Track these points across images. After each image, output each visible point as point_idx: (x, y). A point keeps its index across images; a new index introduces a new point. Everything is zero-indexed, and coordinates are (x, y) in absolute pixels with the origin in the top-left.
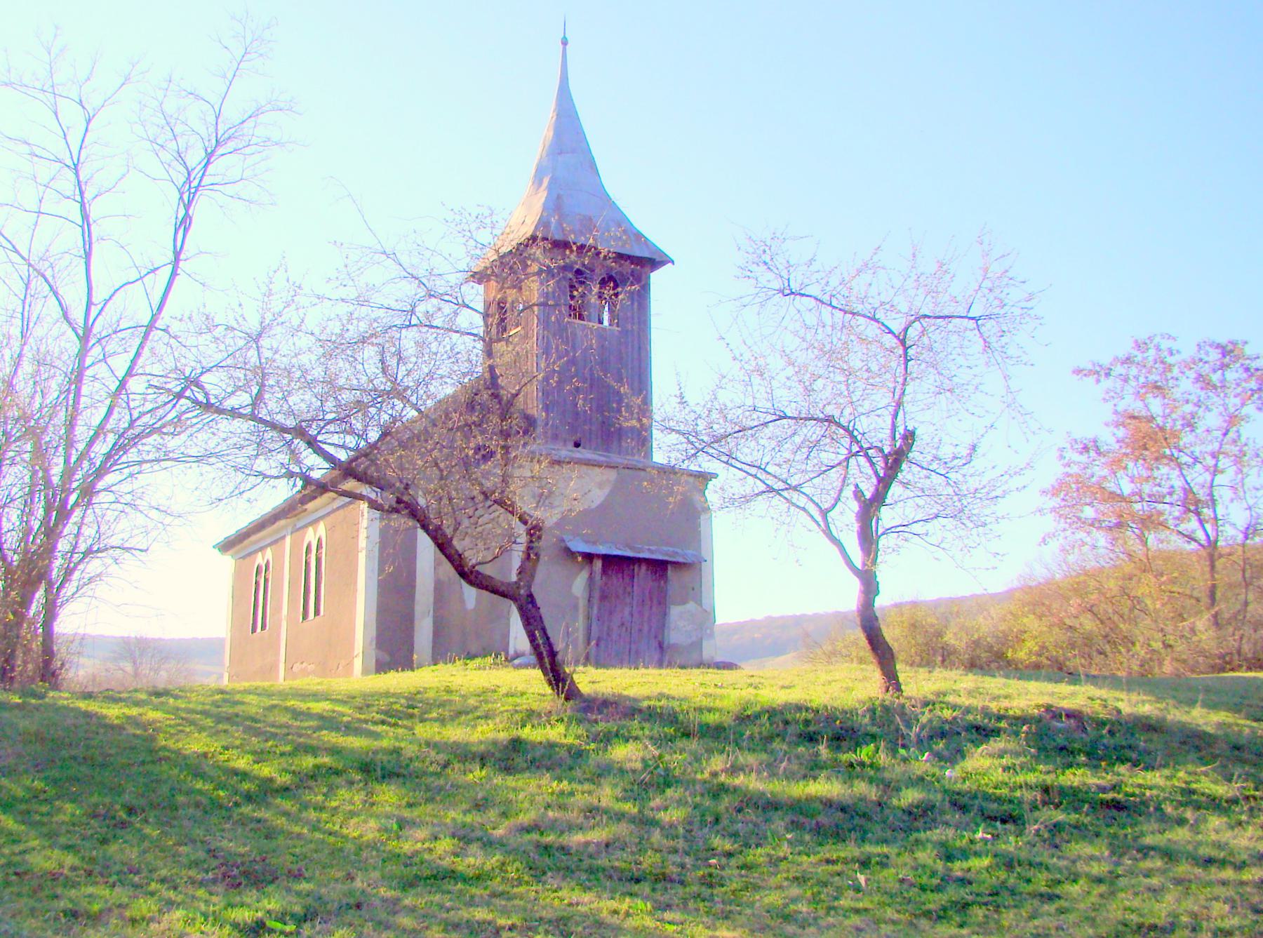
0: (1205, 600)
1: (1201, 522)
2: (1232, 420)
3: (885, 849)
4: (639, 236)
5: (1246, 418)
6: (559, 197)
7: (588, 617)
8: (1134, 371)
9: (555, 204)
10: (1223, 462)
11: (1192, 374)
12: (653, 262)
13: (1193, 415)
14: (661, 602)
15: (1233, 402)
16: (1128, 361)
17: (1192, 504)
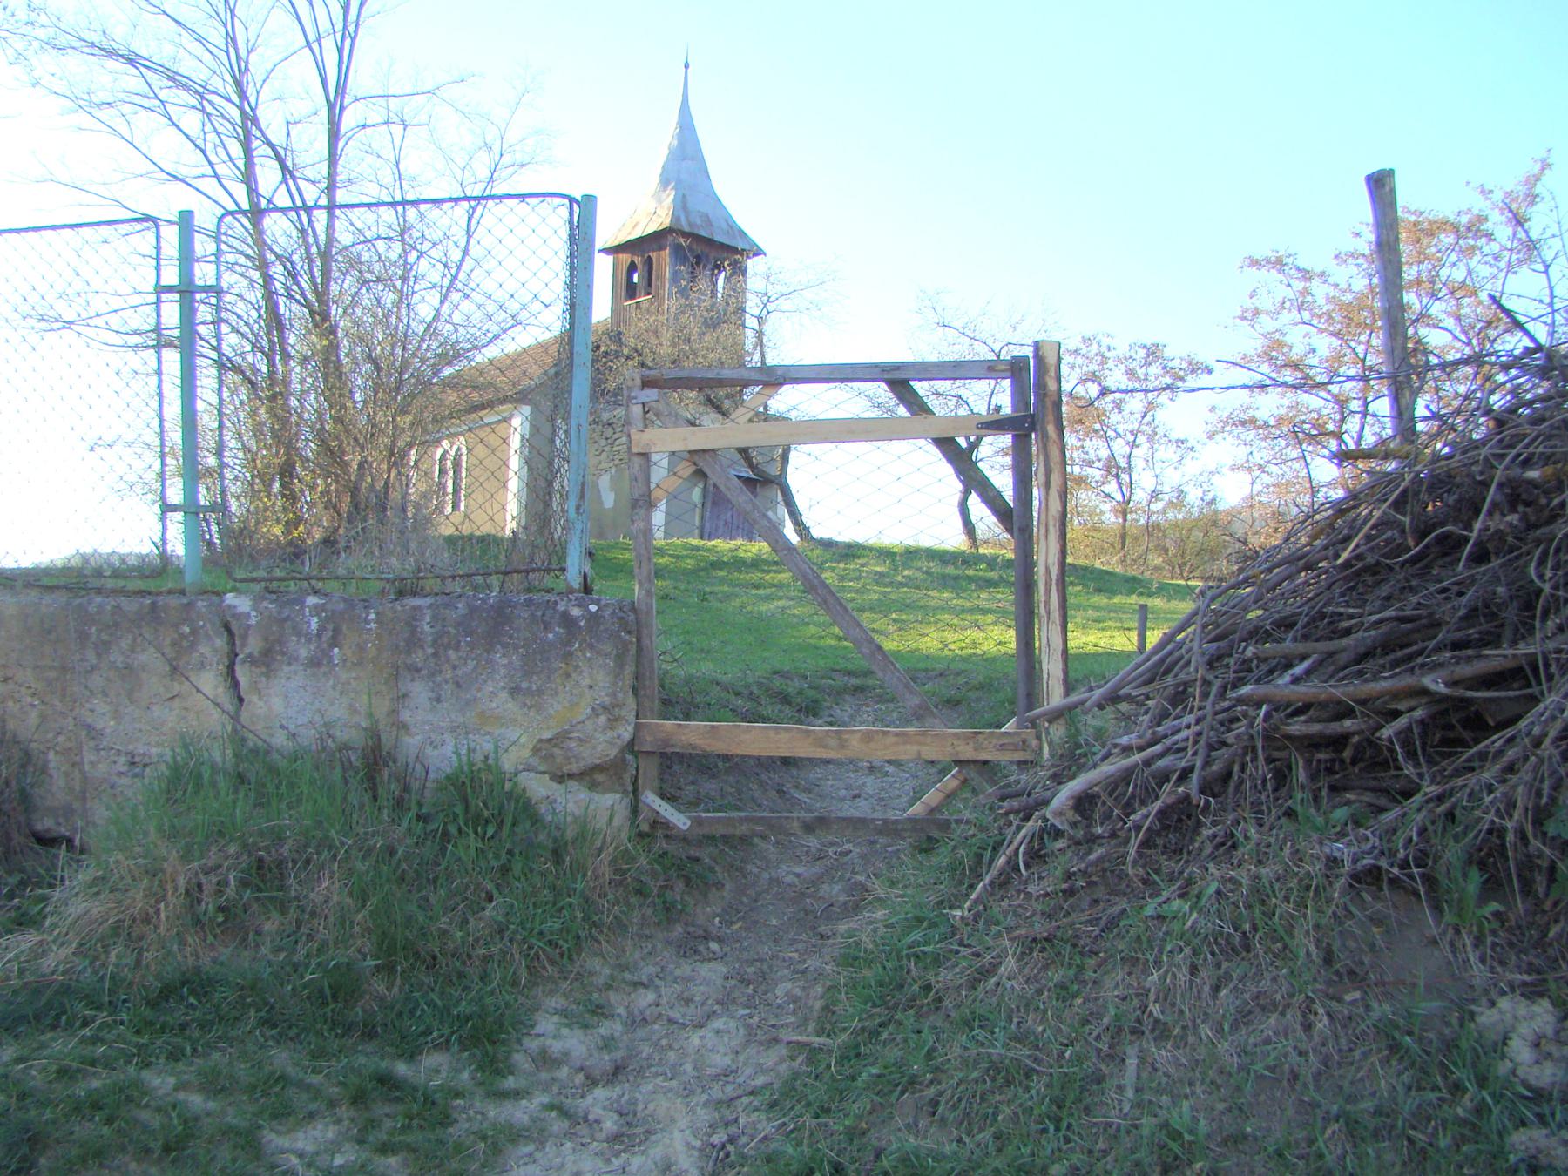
0: (1118, 546)
1: (1120, 484)
4: (742, 234)
6: (684, 196)
7: (702, 518)
8: (1079, 360)
9: (682, 204)
10: (1141, 439)
11: (1123, 368)
17: (1112, 468)
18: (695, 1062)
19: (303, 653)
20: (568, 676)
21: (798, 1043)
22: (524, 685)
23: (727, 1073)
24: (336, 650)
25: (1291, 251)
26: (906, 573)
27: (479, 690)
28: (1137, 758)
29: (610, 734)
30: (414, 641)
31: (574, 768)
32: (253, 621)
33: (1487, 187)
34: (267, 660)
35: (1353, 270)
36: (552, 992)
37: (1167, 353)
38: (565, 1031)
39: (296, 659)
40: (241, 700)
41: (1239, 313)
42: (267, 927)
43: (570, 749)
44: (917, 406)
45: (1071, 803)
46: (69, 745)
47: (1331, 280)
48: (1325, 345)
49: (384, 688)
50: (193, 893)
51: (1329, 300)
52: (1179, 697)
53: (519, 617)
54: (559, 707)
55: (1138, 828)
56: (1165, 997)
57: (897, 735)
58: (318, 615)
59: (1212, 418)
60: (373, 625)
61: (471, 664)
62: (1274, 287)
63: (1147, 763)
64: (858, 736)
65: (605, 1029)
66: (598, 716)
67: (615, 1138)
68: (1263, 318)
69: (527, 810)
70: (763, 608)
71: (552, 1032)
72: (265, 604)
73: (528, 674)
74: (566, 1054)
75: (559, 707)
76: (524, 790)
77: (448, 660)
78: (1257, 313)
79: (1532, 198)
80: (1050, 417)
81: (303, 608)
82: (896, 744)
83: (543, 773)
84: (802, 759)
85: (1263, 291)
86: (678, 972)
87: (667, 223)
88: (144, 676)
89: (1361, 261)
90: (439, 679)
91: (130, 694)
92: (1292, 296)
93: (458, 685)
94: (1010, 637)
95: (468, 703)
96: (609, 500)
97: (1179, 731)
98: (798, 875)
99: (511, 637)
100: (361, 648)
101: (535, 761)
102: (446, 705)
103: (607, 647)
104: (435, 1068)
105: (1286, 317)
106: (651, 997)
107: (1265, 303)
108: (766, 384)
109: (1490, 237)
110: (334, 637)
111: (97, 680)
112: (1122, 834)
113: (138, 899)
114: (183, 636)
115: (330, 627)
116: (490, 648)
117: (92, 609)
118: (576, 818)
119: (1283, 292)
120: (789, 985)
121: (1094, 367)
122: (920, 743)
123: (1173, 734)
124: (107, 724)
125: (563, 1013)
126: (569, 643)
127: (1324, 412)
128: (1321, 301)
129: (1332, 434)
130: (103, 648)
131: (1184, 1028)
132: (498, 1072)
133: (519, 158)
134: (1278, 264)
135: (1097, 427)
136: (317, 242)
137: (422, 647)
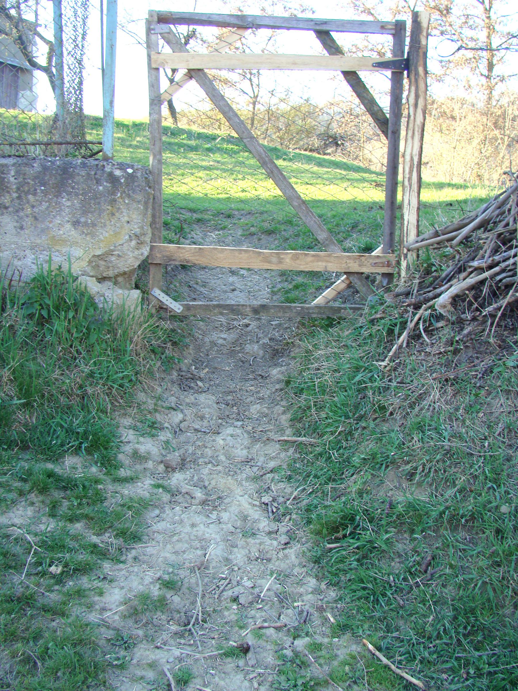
20: (113, 214)
22: (83, 220)
23: (248, 461)
26: (138, 139)
27: (51, 222)
28: (486, 274)
29: (136, 252)
31: (111, 273)
38: (141, 439)
43: (111, 262)
44: (333, 48)
45: (450, 300)
53: (78, 174)
54: (107, 235)
55: (493, 316)
57: (313, 256)
61: (45, 205)
63: (492, 277)
64: (290, 256)
65: (163, 436)
66: (131, 240)
67: (204, 503)
69: (83, 302)
71: (131, 440)
73: (85, 213)
74: (149, 453)
75: (107, 235)
76: (86, 287)
80: (421, 62)
82: (312, 262)
83: (92, 276)
84: (195, 265)
86: (187, 400)
90: (21, 214)
93: (36, 219)
94: (379, 196)
95: (43, 231)
97: (508, 259)
98: (225, 339)
99: (73, 188)
101: (88, 269)
102: (27, 232)
104: (73, 465)
106: (180, 416)
108: (240, 27)
116: (58, 195)
120: (258, 407)
122: (327, 261)
123: (504, 261)
125: (135, 428)
126: (113, 193)
137: (8, 192)
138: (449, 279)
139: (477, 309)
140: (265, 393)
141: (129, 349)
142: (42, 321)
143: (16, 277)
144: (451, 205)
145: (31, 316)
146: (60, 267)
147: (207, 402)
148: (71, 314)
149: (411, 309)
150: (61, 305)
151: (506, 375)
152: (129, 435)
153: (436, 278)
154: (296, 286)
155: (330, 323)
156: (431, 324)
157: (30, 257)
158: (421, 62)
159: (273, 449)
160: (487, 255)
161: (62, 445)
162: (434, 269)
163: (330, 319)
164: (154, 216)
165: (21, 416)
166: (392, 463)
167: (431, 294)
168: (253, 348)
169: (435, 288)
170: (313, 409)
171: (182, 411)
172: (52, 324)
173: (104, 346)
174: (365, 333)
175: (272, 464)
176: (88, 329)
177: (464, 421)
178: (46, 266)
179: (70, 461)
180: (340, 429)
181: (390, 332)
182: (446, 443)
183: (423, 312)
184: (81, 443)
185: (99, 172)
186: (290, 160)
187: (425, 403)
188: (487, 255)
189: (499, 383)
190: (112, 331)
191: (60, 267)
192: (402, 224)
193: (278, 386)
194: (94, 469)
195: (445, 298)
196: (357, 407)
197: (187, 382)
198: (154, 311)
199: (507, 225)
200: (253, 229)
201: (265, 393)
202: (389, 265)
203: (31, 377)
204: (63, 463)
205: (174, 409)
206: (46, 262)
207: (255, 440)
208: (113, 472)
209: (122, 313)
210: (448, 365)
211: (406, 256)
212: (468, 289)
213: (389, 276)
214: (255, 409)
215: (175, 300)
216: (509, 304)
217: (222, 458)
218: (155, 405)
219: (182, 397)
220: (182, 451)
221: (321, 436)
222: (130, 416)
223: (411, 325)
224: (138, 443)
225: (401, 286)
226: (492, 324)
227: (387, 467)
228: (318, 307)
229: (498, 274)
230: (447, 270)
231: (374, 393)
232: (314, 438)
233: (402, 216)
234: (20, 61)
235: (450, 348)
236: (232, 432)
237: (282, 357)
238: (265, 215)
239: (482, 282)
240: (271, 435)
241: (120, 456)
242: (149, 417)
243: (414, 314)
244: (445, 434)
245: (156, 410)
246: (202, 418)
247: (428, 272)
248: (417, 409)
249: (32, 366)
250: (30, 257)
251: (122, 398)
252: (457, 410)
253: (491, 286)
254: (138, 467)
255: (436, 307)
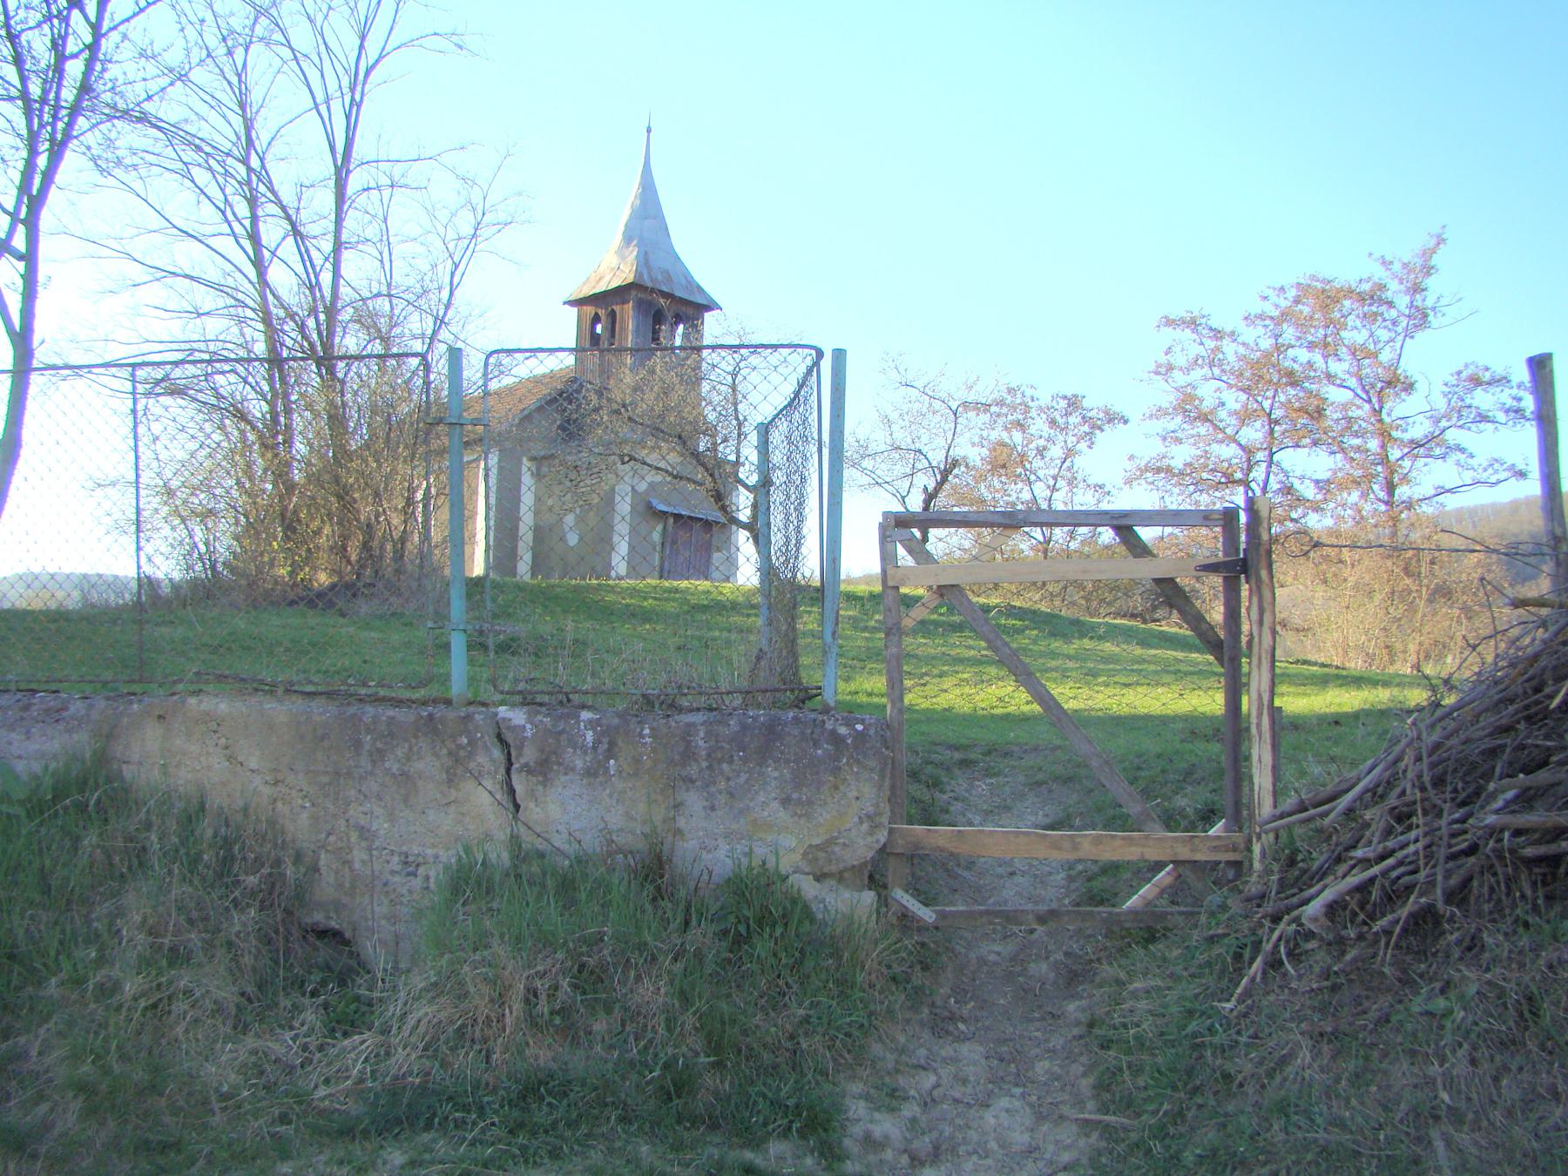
2: (1070, 453)
3: (624, 507)
4: (699, 288)
5: (1079, 453)
9: (644, 261)
10: (1061, 483)
12: (710, 306)
13: (1045, 448)
14: (708, 548)
15: (1071, 440)
16: (1001, 403)
18: (997, 1140)
19: (579, 764)
20: (836, 788)
21: (1086, 1120)
22: (795, 796)
23: (1031, 1151)
24: (612, 762)
25: (1204, 312)
28: (1376, 870)
29: (869, 839)
30: (689, 755)
32: (529, 734)
33: (1388, 258)
34: (543, 769)
35: (1261, 331)
36: (853, 1078)
37: (1086, 403)
38: (877, 1115)
39: (573, 769)
40: (517, 807)
41: (1153, 368)
42: (597, 1027)
46: (340, 844)
47: (1240, 340)
48: (1234, 400)
49: (660, 798)
50: (532, 994)
51: (1241, 358)
52: (1402, 817)
56: (1450, 1083)
57: (1123, 838)
58: (593, 729)
59: (1129, 465)
60: (648, 740)
61: (743, 777)
62: (1189, 345)
63: (1384, 873)
65: (910, 1110)
68: (1176, 374)
69: (798, 909)
70: (1327, 821)
72: (540, 717)
73: (798, 786)
74: (886, 1137)
77: (722, 773)
78: (1170, 368)
79: (1428, 270)
80: (1263, 563)
81: (578, 722)
85: (1177, 349)
86: (943, 1053)
87: (630, 279)
88: (420, 783)
89: (1268, 322)
90: (713, 789)
91: (406, 800)
92: (1204, 353)
93: (731, 795)
95: (741, 812)
96: (573, 539)
97: (1407, 845)
98: (998, 954)
100: (637, 761)
102: (719, 813)
103: (872, 763)
105: (1197, 374)
106: (933, 1079)
107: (1180, 360)
108: (1006, 526)
109: (1390, 304)
110: (609, 750)
111: (373, 786)
112: (1370, 937)
113: (480, 1003)
114: (460, 747)
115: (606, 740)
116: (762, 763)
117: (367, 719)
118: (844, 915)
119: (1196, 350)
120: (1047, 1064)
121: (1018, 416)
123: (1402, 848)
124: (381, 826)
125: (867, 1097)
126: (837, 759)
127: (1234, 461)
128: (1231, 358)
129: (1239, 482)
130: (378, 756)
131: (1476, 1112)
132: (840, 1159)
133: (502, 217)
134: (1192, 324)
135: (1019, 470)
136: (322, 296)
137: (696, 760)
138: (1323, 874)
139: (1365, 923)
140: (1057, 1041)
141: (859, 980)
142: (740, 941)
143: (705, 877)
144: (1336, 723)
145: (725, 932)
146: (764, 863)
147: (972, 1054)
148: (779, 931)
149: (1267, 923)
150: (765, 918)
151: (1409, 1027)
152: (858, 1109)
153: (1304, 872)
154: (1099, 886)
155: (1151, 937)
156: (1297, 945)
157: (724, 848)
158: (1263, 563)
159: (1067, 1133)
160: (1375, 840)
161: (765, 1124)
162: (1300, 857)
163: (1150, 930)
164: (893, 787)
165: (710, 1080)
166: (1242, 1163)
167: (1295, 900)
168: (1040, 969)
169: (1301, 890)
170: (1127, 1073)
171: (935, 1070)
172: (753, 947)
173: (824, 976)
174: (1202, 958)
175: (1066, 1157)
176: (802, 951)
177: (1347, 1100)
178: (745, 861)
179: (776, 1147)
180: (1165, 1107)
181: (1238, 957)
182: (1321, 1135)
183: (1285, 927)
184: (791, 1122)
185: (817, 731)
186: (1100, 638)
187: (1290, 1070)
188: (1375, 840)
189: (1399, 1039)
190: (836, 955)
191: (764, 863)
192: (1252, 790)
193: (1076, 1031)
194: (809, 1161)
195: (1314, 908)
196: (1190, 1072)
197: (942, 1025)
198: (894, 921)
199: (1403, 793)
200: (1040, 776)
201: (1057, 1041)
202: (1235, 849)
203: (723, 1023)
204: (767, 1151)
205: (924, 1069)
206: (745, 854)
207: (1040, 1117)
208: (835, 1165)
209: (849, 926)
210: (1323, 1009)
211: (1259, 837)
212: (1350, 892)
213: (1237, 865)
214: (1042, 1067)
215: (926, 905)
216: (1412, 915)
217: (993, 1145)
218: (897, 1062)
219: (936, 1048)
220: (935, 1134)
221: (1138, 1115)
222: (861, 1079)
223: (1267, 947)
224: (871, 1122)
225: (1253, 886)
226: (1387, 944)
227: (1234, 1169)
228: (1133, 912)
229: (1393, 868)
230: (1319, 859)
231: (1214, 1054)
232: (1128, 1117)
233: (1251, 777)
234: (714, 514)
235: (1326, 983)
236: (1008, 1105)
237: (1082, 983)
238: (1059, 753)
239: (1372, 880)
240: (1065, 1110)
241: (847, 1142)
242: (887, 1080)
243: (1272, 930)
244: (1319, 1120)
245: (898, 1071)
246: (965, 1082)
247: (1292, 862)
248: (1278, 1079)
249: (724, 1006)
250: (724, 848)
251: (849, 1052)
252: (1338, 1080)
253: (1383, 886)
254: (872, 1158)
255: (1303, 920)
